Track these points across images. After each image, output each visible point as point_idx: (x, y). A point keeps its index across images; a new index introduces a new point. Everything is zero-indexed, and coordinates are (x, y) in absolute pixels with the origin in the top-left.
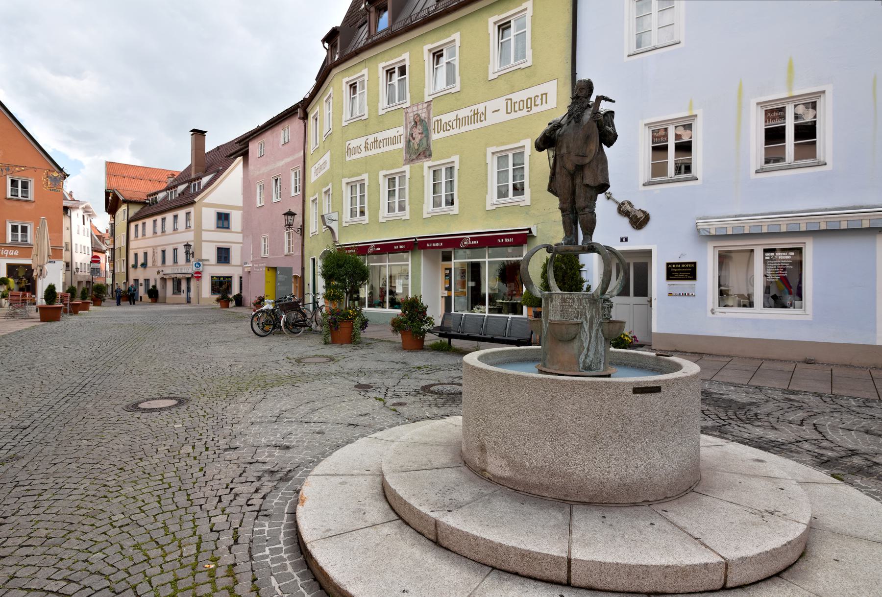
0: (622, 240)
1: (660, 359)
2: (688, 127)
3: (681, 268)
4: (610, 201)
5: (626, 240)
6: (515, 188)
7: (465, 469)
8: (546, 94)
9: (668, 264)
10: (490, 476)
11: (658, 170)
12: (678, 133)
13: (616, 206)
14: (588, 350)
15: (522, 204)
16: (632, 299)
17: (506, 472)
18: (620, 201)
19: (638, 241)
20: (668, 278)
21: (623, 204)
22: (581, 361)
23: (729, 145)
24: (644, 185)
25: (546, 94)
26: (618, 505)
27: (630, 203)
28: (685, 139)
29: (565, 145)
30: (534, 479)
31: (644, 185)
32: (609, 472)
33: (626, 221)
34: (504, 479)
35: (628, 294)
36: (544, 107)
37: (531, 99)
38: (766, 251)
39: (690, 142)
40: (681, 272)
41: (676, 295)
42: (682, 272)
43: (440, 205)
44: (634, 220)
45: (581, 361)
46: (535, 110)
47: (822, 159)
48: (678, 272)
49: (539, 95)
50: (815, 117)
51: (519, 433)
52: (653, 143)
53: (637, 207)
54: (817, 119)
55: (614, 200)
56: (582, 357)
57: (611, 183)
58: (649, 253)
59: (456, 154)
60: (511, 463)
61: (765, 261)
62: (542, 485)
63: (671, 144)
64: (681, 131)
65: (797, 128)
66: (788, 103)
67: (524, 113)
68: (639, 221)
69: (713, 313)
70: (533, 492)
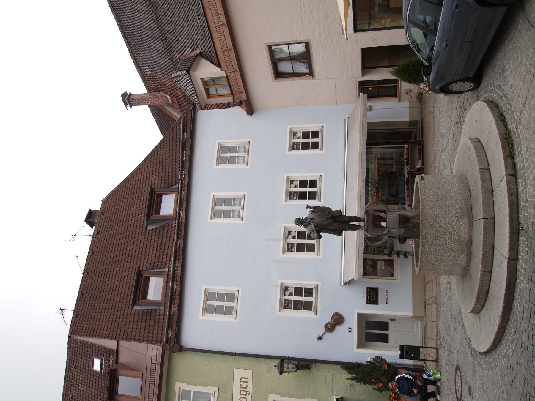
0: (350, 332)
2: (286, 288)
3: (370, 296)
4: (324, 337)
5: (350, 328)
8: (242, 378)
9: (367, 303)
11: (308, 306)
13: (328, 334)
16: (390, 332)
17: (465, 220)
18: (324, 330)
19: (352, 322)
24: (316, 314)
25: (242, 378)
31: (316, 314)
33: (338, 328)
35: (387, 335)
36: (250, 381)
37: (241, 391)
39: (298, 232)
41: (387, 300)
46: (249, 389)
55: (323, 335)
58: (360, 316)
59: (267, 396)
64: (288, 293)
65: (296, 295)
66: (282, 298)
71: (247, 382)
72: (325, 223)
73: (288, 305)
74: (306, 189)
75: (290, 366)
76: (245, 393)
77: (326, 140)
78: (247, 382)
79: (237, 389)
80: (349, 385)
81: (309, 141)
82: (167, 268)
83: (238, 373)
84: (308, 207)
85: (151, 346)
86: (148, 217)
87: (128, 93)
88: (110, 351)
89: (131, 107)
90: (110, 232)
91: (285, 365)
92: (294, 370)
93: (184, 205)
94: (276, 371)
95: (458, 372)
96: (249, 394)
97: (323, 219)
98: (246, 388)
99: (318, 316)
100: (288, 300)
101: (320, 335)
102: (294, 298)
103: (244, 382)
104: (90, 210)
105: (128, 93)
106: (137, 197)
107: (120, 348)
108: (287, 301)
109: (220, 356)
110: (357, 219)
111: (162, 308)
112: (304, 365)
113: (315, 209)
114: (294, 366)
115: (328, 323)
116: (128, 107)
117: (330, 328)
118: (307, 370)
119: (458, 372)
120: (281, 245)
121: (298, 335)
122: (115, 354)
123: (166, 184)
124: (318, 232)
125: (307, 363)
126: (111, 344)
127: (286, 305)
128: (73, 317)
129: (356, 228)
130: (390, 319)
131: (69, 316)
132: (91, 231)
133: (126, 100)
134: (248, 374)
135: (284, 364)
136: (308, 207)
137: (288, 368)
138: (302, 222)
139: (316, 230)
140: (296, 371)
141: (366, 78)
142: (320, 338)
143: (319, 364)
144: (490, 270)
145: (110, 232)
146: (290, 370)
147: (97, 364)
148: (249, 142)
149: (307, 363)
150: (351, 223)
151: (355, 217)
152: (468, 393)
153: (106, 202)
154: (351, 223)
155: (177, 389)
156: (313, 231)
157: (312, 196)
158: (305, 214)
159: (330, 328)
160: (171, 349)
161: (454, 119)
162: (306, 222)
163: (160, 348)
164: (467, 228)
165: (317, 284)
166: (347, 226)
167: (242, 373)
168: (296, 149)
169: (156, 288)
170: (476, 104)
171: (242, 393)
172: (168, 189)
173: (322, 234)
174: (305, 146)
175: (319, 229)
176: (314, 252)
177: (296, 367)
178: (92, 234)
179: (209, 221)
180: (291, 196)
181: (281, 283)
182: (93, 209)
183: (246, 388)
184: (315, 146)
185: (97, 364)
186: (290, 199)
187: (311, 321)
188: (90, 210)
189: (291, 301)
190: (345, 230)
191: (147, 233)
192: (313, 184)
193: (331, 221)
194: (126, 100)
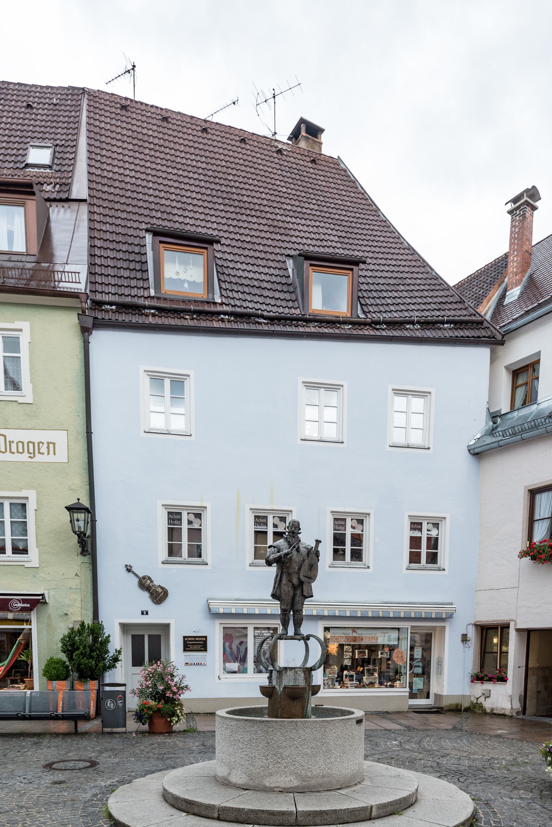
0: (142, 613)
1: (318, 708)
4: (131, 574)
5: (147, 613)
6: (353, 552)
8: (54, 444)
9: (184, 637)
11: (173, 550)
13: (137, 580)
15: (27, 565)
17: (295, 783)
18: (141, 576)
19: (158, 615)
20: (185, 650)
21: (144, 578)
23: (386, 542)
24: (163, 563)
25: (54, 444)
26: (351, 823)
27: (149, 578)
28: (196, 526)
33: (146, 595)
36: (51, 458)
37: (34, 443)
38: (256, 628)
40: (196, 644)
41: (191, 665)
42: (196, 644)
43: (419, 562)
46: (38, 458)
47: (205, 560)
49: (45, 441)
51: (304, 756)
52: (334, 530)
53: (156, 583)
54: (439, 536)
58: (167, 626)
60: (298, 776)
61: (255, 636)
63: (270, 530)
67: (25, 457)
68: (159, 596)
69: (219, 679)
71: (48, 454)
74: (349, 545)
75: (81, 524)
76: (31, 450)
77: (425, 575)
78: (48, 454)
79: (36, 436)
80: (65, 612)
81: (424, 550)
82: (219, 301)
83: (60, 438)
84: (318, 542)
85: (83, 270)
86: (307, 257)
87: (537, 204)
88: (67, 185)
89: (510, 212)
90: (281, 178)
91: (81, 516)
92: (77, 529)
93: (329, 328)
94: (72, 501)
95: (89, 764)
96: (30, 457)
98: (39, 453)
100: (180, 520)
101: (134, 569)
102: (185, 527)
103: (48, 448)
104: (322, 131)
105: (537, 204)
106: (344, 234)
107: (75, 205)
109: (83, 405)
111: (152, 293)
112: (87, 544)
113: (314, 554)
114: (82, 530)
115: (152, 581)
116: (510, 206)
117: (145, 584)
118: (80, 550)
119: (89, 764)
120: (264, 504)
121: (131, 535)
122: (64, 196)
123: (365, 294)
124: (279, 561)
125: (89, 550)
126: (80, 188)
128: (121, 98)
131: (122, 89)
132: (283, 135)
133: (526, 198)
134: (61, 456)
135: (83, 511)
136: (318, 542)
137: (78, 520)
139: (280, 557)
140: (75, 532)
141: (513, 635)
142: (129, 569)
143: (91, 568)
144: (221, 818)
145: (281, 178)
146: (76, 523)
147: (40, 156)
149: (89, 550)
152: (56, 779)
153: (336, 165)
155: (17, 325)
156: (279, 552)
157: (338, 554)
158: (307, 539)
159: (145, 584)
160: (84, 312)
161: (444, 761)
163: (81, 287)
164: (283, 786)
165: (207, 564)
167: (63, 445)
169: (183, 274)
170: (467, 797)
171: (31, 445)
172: (355, 298)
174: (415, 542)
175: (281, 562)
177: (81, 532)
178: (277, 137)
180: (339, 521)
182: (324, 138)
183: (39, 453)
184: (414, 558)
185: (40, 156)
186: (335, 519)
187: (151, 555)
188: (322, 131)
189: (181, 524)
190: (281, 604)
191: (279, 258)
192: (357, 555)
193: (295, 581)
194: (526, 198)
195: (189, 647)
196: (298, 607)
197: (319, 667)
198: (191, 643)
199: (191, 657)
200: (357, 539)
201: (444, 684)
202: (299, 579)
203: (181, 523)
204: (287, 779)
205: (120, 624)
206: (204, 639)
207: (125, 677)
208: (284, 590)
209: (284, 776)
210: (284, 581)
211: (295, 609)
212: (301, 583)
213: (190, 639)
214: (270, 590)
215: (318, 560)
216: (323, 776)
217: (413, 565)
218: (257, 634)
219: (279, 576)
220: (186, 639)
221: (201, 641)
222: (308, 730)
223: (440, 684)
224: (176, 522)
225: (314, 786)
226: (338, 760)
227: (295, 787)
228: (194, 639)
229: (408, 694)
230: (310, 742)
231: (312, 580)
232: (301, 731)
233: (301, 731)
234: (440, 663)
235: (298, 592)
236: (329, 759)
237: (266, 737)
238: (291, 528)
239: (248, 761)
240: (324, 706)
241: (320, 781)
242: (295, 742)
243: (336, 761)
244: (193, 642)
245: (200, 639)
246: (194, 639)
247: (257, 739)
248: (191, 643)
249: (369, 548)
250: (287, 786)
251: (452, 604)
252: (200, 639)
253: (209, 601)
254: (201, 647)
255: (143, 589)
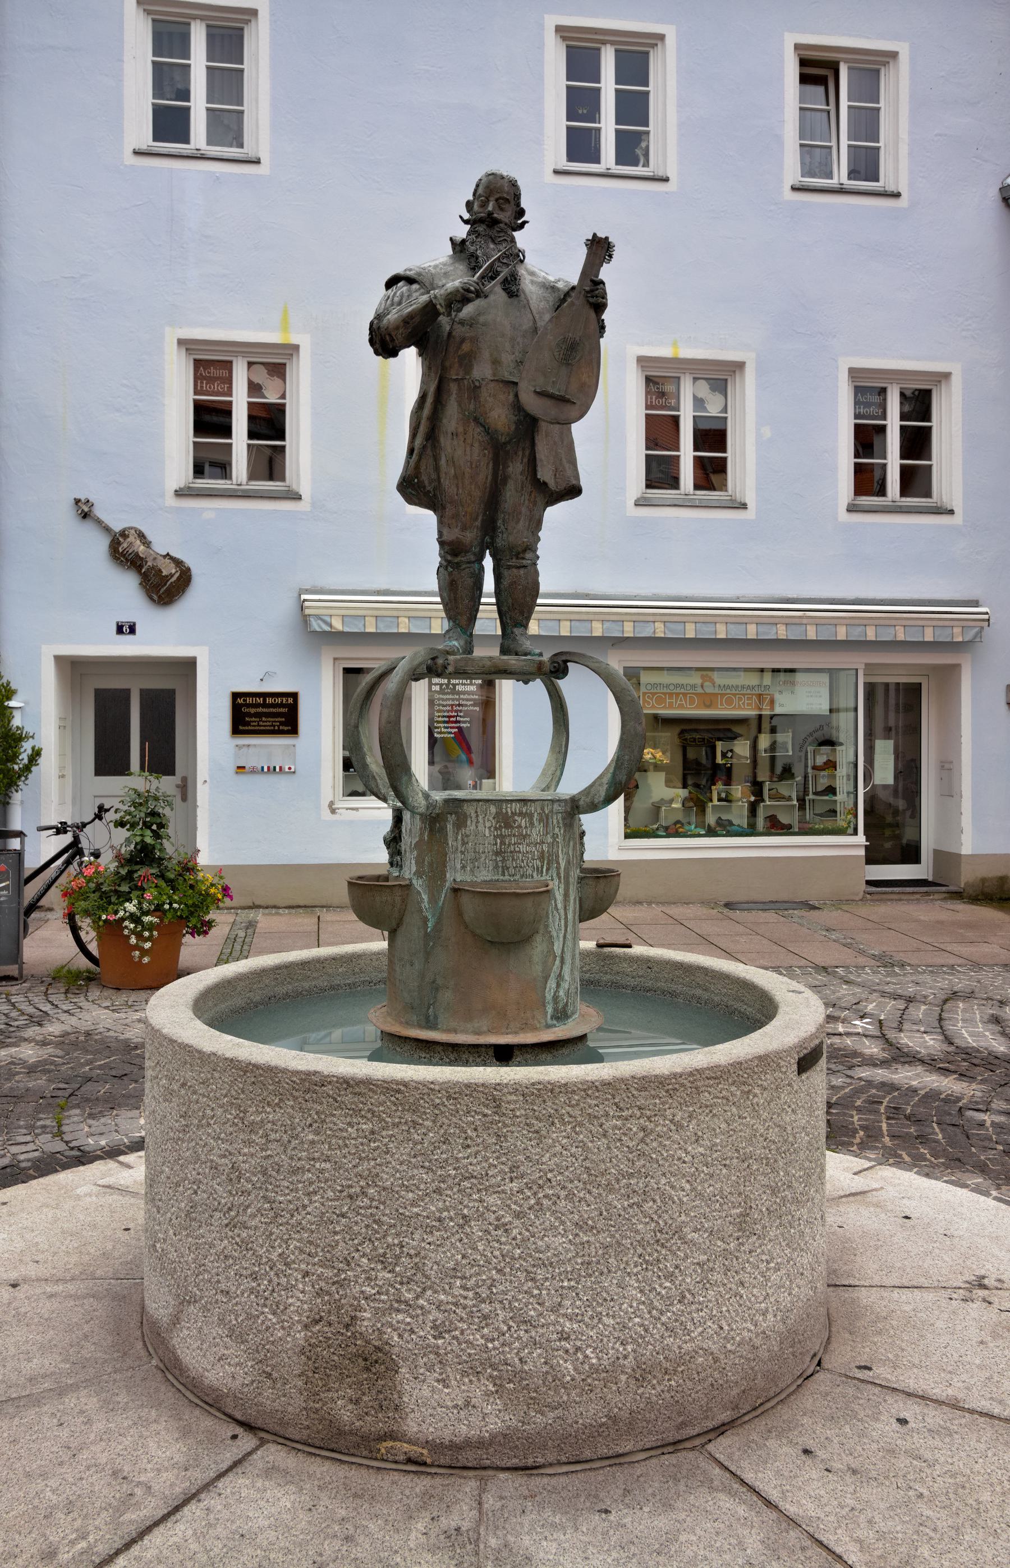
0: (120, 630)
2: (278, 370)
4: (88, 526)
5: (132, 630)
7: (273, 1454)
9: (235, 696)
10: (414, 1450)
11: (209, 464)
12: (256, 380)
13: (103, 544)
14: (562, 962)
17: (492, 1418)
18: (117, 527)
19: (161, 635)
21: (124, 534)
22: (549, 996)
27: (141, 536)
28: (272, 398)
29: (486, 354)
30: (589, 1411)
31: (179, 493)
32: (765, 1313)
33: (126, 586)
34: (481, 1444)
40: (269, 715)
41: (253, 771)
44: (154, 580)
45: (549, 996)
48: (256, 715)
50: (725, 410)
51: (540, 1273)
55: (99, 522)
56: (552, 984)
57: (583, 483)
58: (188, 666)
60: (508, 1381)
62: (614, 1419)
64: (261, 376)
66: (237, 354)
68: (166, 585)
69: (333, 811)
70: (588, 1454)
72: (482, 371)
73: (211, 380)
97: (507, 359)
99: (171, 501)
101: (99, 512)
108: (224, 373)
110: (518, 602)
115: (147, 543)
117: (126, 553)
127: (210, 366)
129: (459, 596)
130: (184, 779)
136: (600, 249)
138: (491, 222)
139: (430, 311)
142: (85, 512)
148: (744, 506)
150: (488, 563)
151: (534, 590)
154: (488, 563)
159: (126, 553)
162: (491, 254)
166: (470, 536)
168: (857, 403)
173: (410, 357)
176: (154, 140)
179: (552, 21)
181: (296, 348)
193: (500, 417)
195: (248, 724)
196: (510, 535)
197: (609, 800)
198: (253, 711)
199: (251, 750)
200: (712, 438)
201: (963, 824)
202: (517, 406)
203: (230, 388)
204: (453, 1395)
205: (59, 659)
206: (291, 701)
207: (74, 804)
208: (452, 461)
209: (432, 1377)
210: (452, 418)
211: (500, 542)
212: (528, 426)
213: (249, 700)
214: (395, 461)
215: (602, 328)
216: (642, 1375)
217: (866, 500)
218: (437, 688)
219: (430, 400)
220: (240, 701)
221: (282, 705)
222: (558, 1135)
223: (950, 821)
224: (216, 386)
225: (595, 1432)
226: (716, 1277)
227: (493, 1436)
228: (261, 701)
229: (862, 852)
230: (570, 1197)
231: (573, 412)
232: (518, 1139)
233: (518, 1139)
234: (948, 768)
235: (516, 468)
236: (670, 1276)
237: (338, 1166)
238: (484, 205)
239: (254, 1277)
240: (638, 950)
241: (623, 1399)
242: (492, 1200)
243: (705, 1283)
244: (260, 710)
245: (279, 700)
246: (261, 701)
247: (295, 1171)
248: (253, 711)
249: (743, 455)
250: (447, 1435)
251: (976, 603)
252: (279, 700)
253: (304, 597)
254: (282, 723)
255: (121, 564)
